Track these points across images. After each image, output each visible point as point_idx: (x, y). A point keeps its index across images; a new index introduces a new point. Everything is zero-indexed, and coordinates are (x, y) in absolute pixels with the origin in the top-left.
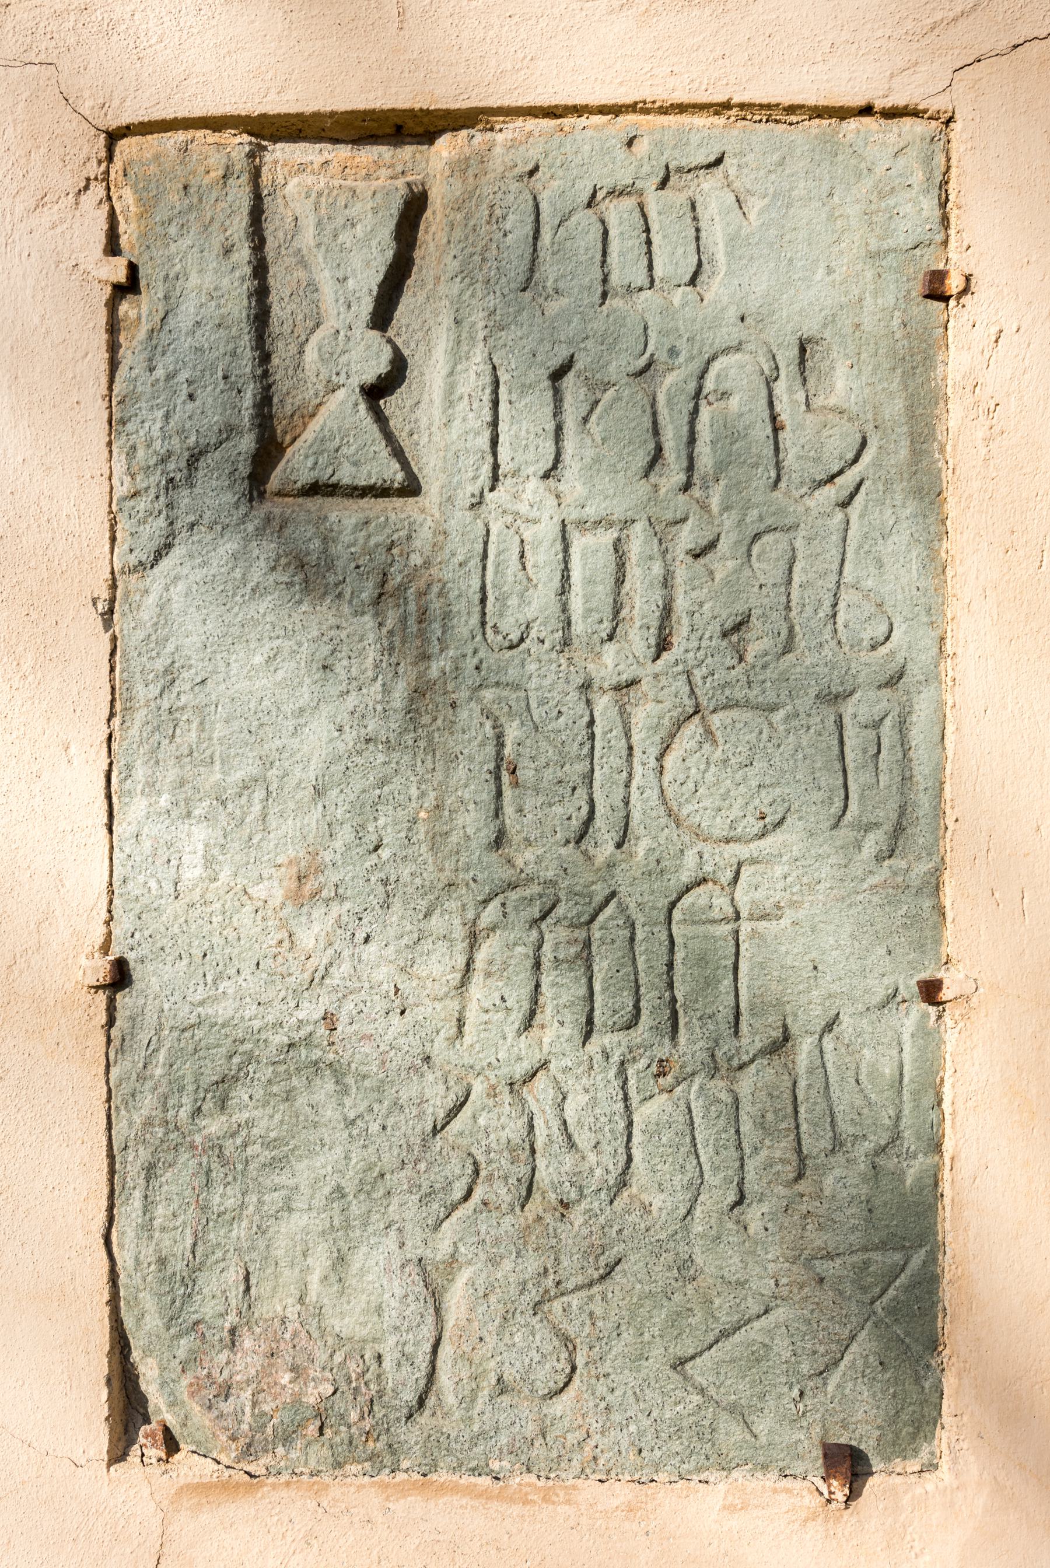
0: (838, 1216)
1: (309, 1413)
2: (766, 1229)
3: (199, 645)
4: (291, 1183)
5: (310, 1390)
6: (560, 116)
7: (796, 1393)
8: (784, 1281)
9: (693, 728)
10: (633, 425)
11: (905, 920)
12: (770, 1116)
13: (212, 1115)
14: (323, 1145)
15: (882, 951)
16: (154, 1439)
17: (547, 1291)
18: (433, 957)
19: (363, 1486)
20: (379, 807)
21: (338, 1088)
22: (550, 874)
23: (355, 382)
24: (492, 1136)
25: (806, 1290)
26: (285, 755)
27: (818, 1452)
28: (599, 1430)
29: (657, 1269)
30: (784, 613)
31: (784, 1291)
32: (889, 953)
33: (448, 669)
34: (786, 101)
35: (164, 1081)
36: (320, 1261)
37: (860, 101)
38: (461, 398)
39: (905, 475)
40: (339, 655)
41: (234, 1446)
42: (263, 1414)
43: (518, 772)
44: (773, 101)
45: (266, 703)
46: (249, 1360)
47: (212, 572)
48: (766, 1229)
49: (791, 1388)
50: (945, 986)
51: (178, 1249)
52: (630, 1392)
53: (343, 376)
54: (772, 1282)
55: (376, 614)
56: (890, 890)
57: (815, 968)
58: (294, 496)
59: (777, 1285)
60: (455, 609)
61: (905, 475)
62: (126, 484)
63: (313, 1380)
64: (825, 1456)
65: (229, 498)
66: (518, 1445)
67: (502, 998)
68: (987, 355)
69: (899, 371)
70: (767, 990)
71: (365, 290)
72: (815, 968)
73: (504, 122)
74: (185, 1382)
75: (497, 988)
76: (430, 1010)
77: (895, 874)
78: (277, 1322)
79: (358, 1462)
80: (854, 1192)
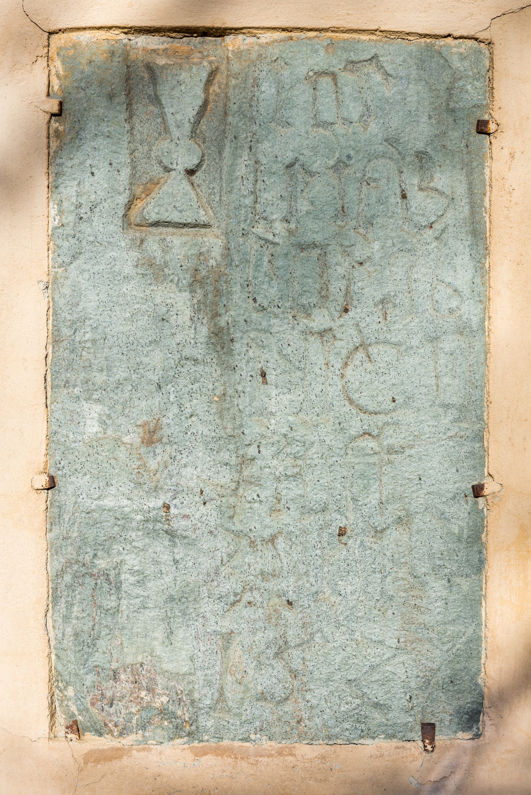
0: (431, 607)
1: (156, 712)
2: (394, 614)
3: (95, 307)
4: (145, 594)
5: (156, 700)
6: (291, 31)
7: (408, 697)
8: (402, 640)
9: (360, 355)
10: (328, 194)
11: (466, 454)
12: (396, 556)
13: (102, 558)
14: (162, 574)
15: (454, 470)
16: (72, 729)
17: (280, 647)
18: (221, 475)
19: (184, 749)
20: (193, 395)
21: (170, 544)
22: (283, 431)
23: (180, 168)
24: (252, 568)
25: (414, 644)
26: (141, 367)
27: (418, 728)
28: (307, 718)
29: (338, 635)
30: (345, 360)
31: (402, 645)
32: (457, 471)
33: (230, 321)
34: (407, 30)
35: (78, 540)
36: (159, 634)
37: (446, 34)
38: (237, 178)
39: (468, 224)
40: (172, 313)
41: (116, 730)
42: (131, 713)
43: (266, 376)
44: (400, 30)
45: (131, 338)
46: (124, 685)
47: (102, 268)
48: (394, 614)
49: (405, 695)
50: (485, 488)
51: (86, 628)
52: (323, 698)
53: (175, 165)
54: (397, 640)
55: (191, 292)
56: (459, 439)
57: (420, 479)
58: (147, 226)
59: (399, 642)
60: (234, 290)
61: (468, 224)
62: (57, 221)
63: (158, 694)
64: (422, 728)
65: (358, 353)
66: (265, 726)
67: (258, 495)
68: (509, 164)
69: (465, 170)
70: (395, 491)
71: (187, 120)
72: (420, 479)
73: (260, 33)
74: (89, 698)
75: (255, 491)
76: (219, 502)
77: (461, 430)
78: (138, 666)
79: (181, 737)
80: (439, 594)
